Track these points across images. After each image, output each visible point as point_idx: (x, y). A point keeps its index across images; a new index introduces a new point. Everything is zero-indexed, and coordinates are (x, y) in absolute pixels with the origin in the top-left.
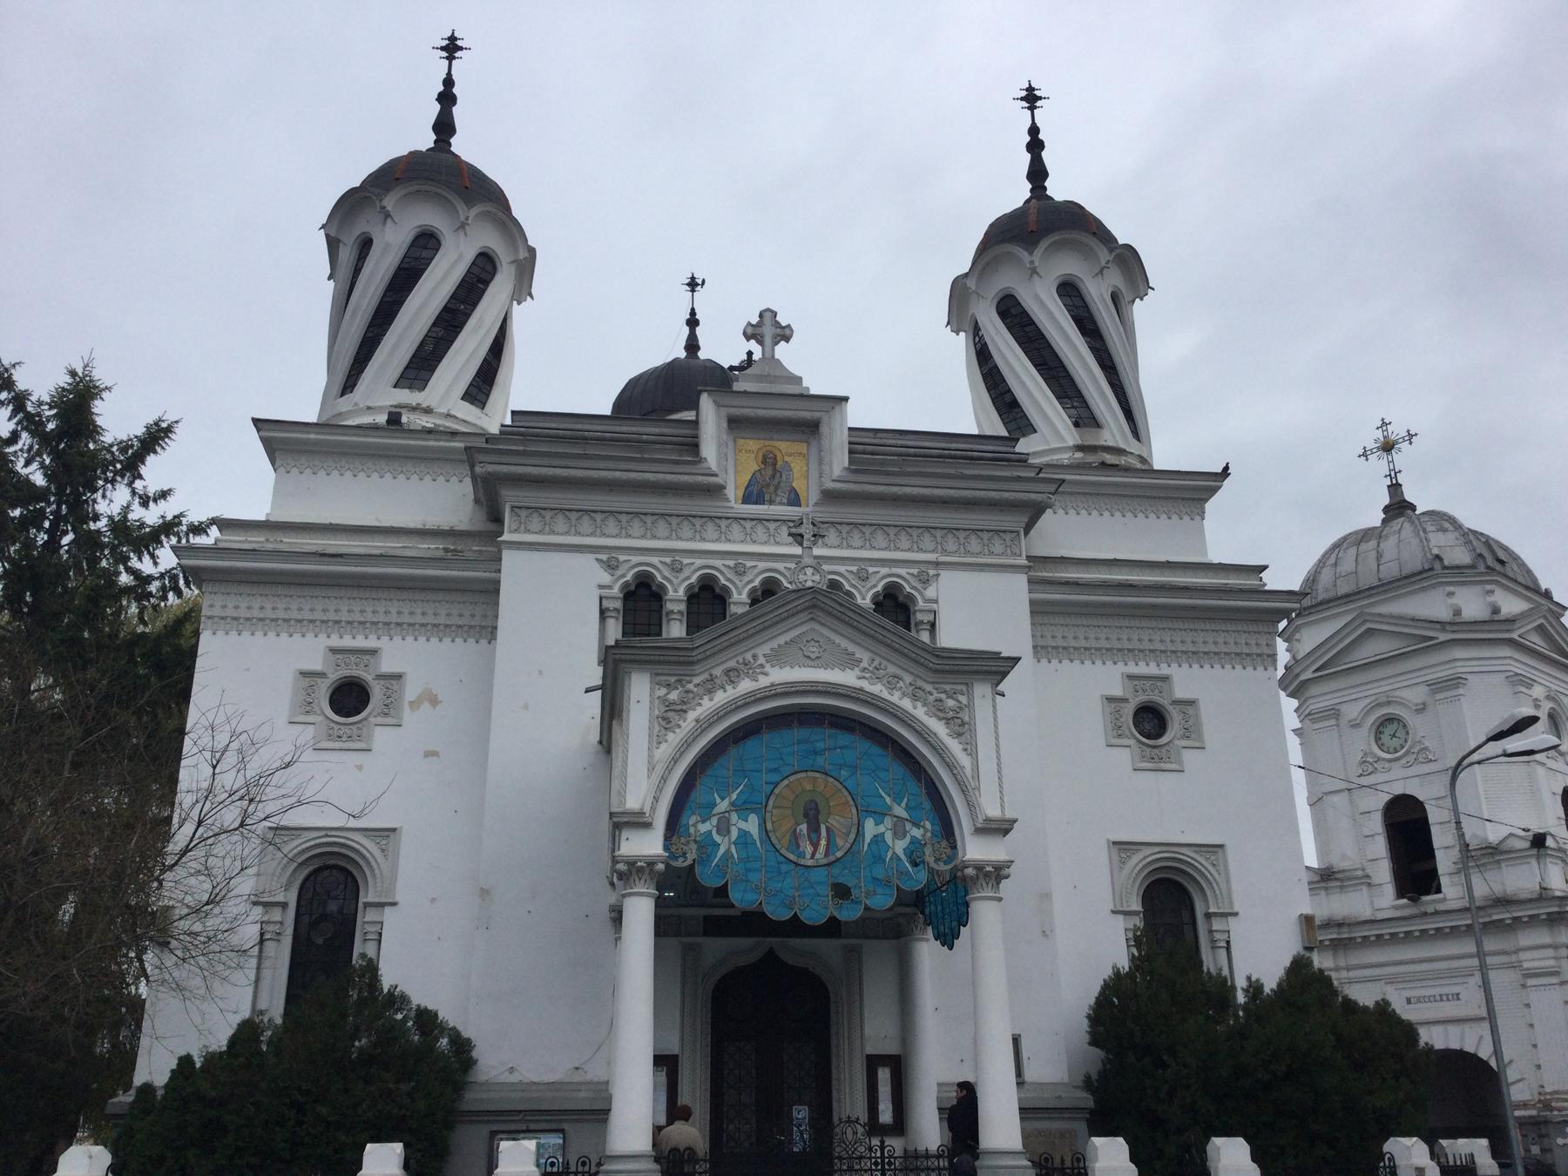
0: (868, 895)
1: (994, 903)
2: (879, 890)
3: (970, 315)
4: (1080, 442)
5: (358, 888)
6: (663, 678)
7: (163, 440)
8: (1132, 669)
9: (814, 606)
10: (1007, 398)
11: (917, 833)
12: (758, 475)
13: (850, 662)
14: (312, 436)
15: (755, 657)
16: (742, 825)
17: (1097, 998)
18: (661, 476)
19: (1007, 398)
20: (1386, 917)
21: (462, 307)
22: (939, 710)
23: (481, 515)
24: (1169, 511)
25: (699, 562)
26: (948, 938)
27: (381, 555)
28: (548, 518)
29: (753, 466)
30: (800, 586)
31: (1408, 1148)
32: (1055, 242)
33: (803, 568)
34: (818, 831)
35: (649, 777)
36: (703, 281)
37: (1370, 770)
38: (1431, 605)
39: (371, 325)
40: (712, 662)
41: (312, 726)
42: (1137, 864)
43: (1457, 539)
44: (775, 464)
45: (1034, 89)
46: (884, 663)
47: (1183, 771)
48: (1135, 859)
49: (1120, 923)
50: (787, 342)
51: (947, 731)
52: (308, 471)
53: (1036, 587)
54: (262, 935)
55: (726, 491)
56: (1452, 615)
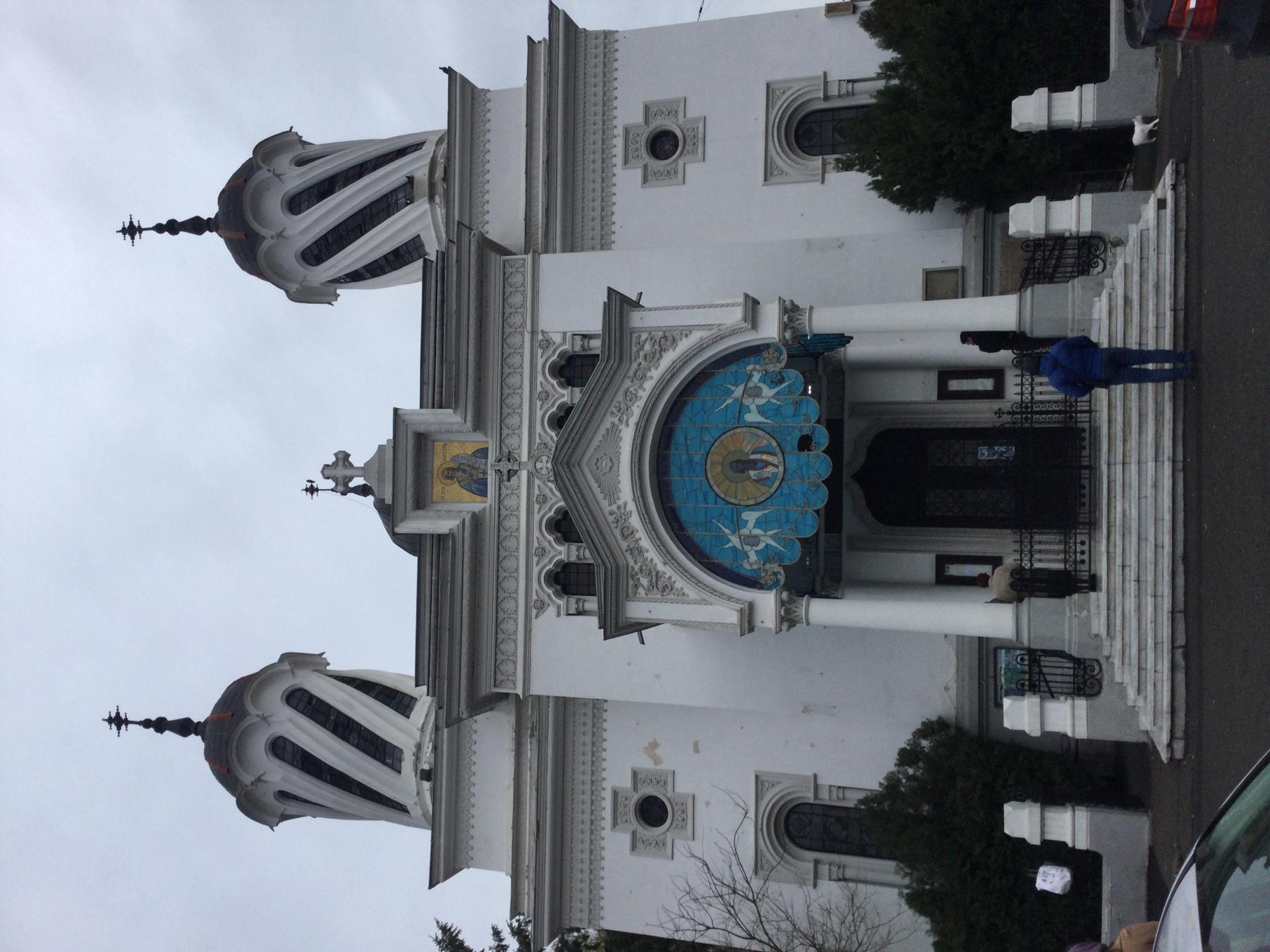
0: (807, 420)
2: (803, 410)
4: (426, 198)
5: (799, 805)
6: (630, 591)
7: (452, 933)
8: (619, 160)
9: (568, 464)
10: (391, 258)
11: (756, 377)
12: (462, 483)
13: (614, 433)
15: (611, 513)
16: (751, 525)
18: (466, 566)
19: (391, 258)
21: (332, 718)
22: (653, 358)
23: (503, 705)
24: (483, 151)
25: (536, 533)
27: (537, 790)
28: (504, 657)
29: (455, 489)
30: (552, 473)
33: (536, 470)
35: (711, 604)
36: (309, 481)
41: (676, 841)
44: (453, 469)
45: (124, 228)
46: (614, 403)
50: (350, 455)
51: (671, 350)
52: (471, 842)
54: (839, 880)
55: (477, 511)
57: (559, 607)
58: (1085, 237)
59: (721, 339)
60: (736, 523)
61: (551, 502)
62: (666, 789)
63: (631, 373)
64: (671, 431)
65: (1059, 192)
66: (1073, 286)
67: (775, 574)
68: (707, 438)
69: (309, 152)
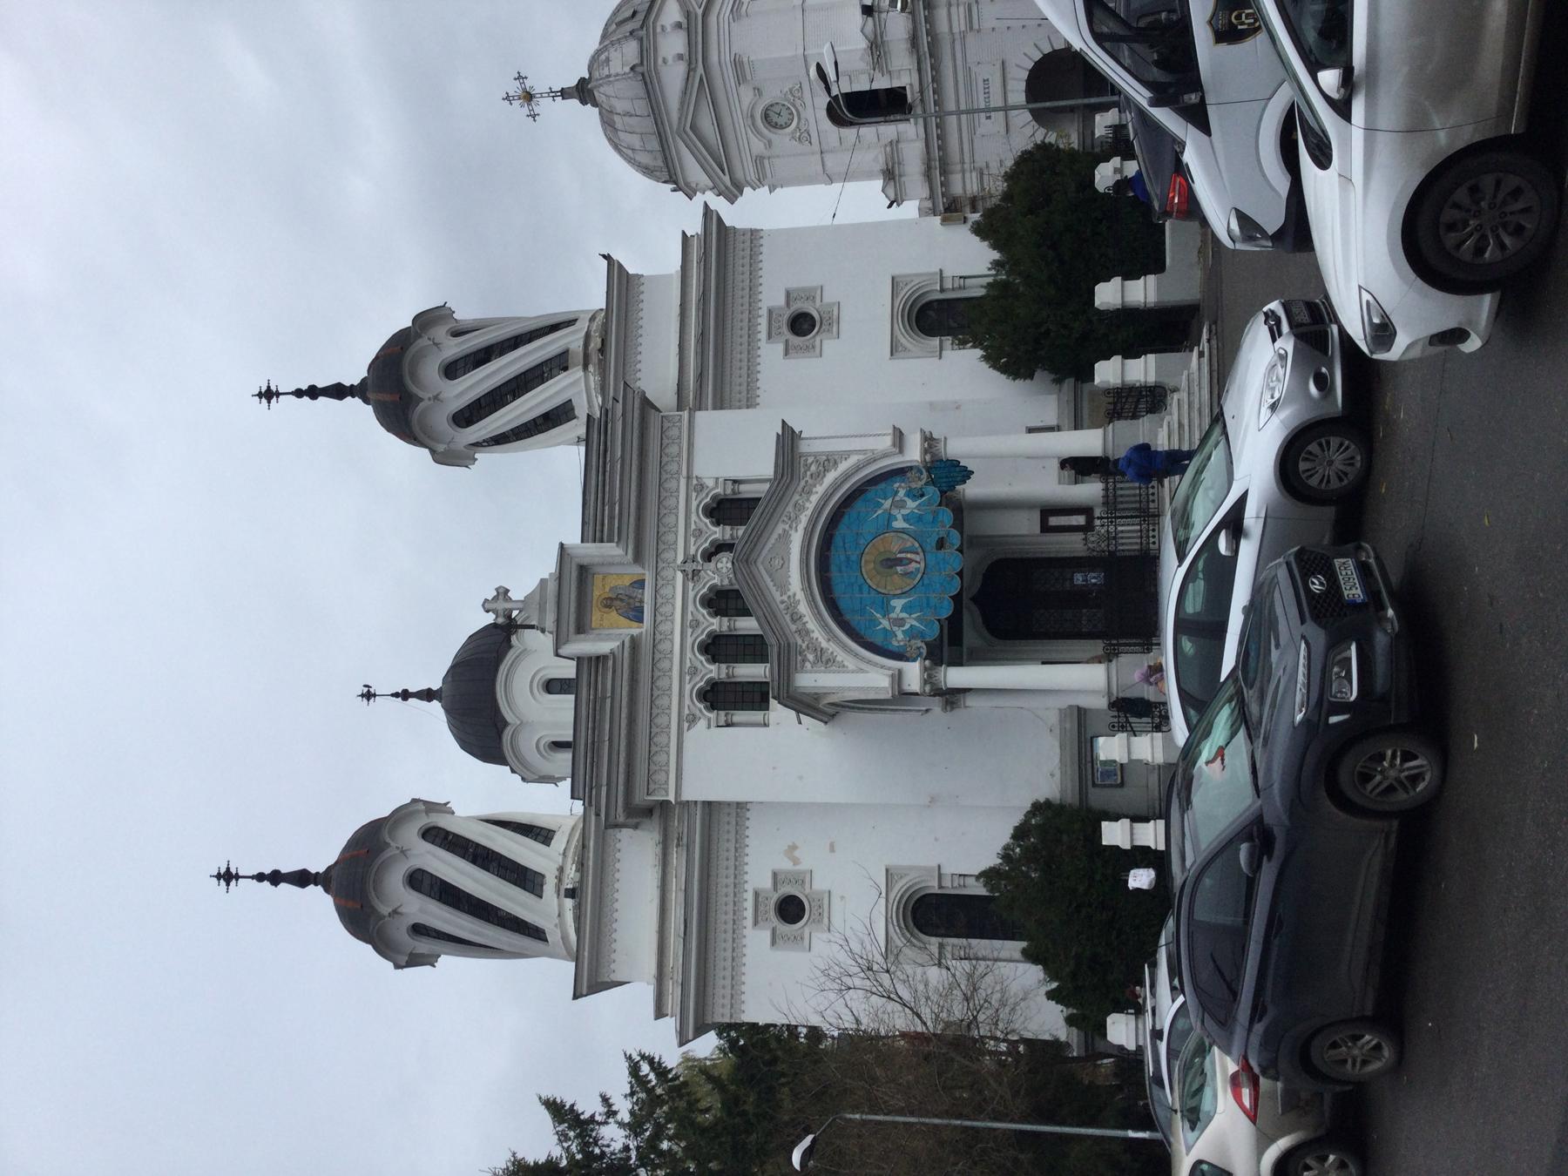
1: (948, 441)
3: (464, 450)
4: (581, 367)
6: (799, 665)
8: (763, 335)
9: (747, 561)
11: (902, 493)
13: (786, 537)
14: (586, 954)
15: (782, 602)
16: (898, 609)
17: (1002, 373)
20: (923, 130)
26: (966, 474)
31: (1102, 177)
32: (411, 378)
34: (901, 559)
36: (365, 686)
37: (806, 135)
38: (673, 78)
39: (488, 920)
40: (787, 632)
41: (813, 934)
42: (907, 339)
43: (616, 50)
44: (611, 599)
45: (260, 392)
46: (785, 513)
47: (839, 303)
48: (903, 340)
49: (947, 353)
53: (703, 406)
56: (681, 62)
57: (709, 720)
58: (1151, 387)
59: (875, 461)
60: (885, 609)
61: (704, 626)
62: (803, 887)
63: (800, 489)
64: (831, 536)
65: (1131, 352)
66: (1143, 421)
67: (919, 648)
68: (862, 541)
69: (460, 327)
